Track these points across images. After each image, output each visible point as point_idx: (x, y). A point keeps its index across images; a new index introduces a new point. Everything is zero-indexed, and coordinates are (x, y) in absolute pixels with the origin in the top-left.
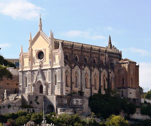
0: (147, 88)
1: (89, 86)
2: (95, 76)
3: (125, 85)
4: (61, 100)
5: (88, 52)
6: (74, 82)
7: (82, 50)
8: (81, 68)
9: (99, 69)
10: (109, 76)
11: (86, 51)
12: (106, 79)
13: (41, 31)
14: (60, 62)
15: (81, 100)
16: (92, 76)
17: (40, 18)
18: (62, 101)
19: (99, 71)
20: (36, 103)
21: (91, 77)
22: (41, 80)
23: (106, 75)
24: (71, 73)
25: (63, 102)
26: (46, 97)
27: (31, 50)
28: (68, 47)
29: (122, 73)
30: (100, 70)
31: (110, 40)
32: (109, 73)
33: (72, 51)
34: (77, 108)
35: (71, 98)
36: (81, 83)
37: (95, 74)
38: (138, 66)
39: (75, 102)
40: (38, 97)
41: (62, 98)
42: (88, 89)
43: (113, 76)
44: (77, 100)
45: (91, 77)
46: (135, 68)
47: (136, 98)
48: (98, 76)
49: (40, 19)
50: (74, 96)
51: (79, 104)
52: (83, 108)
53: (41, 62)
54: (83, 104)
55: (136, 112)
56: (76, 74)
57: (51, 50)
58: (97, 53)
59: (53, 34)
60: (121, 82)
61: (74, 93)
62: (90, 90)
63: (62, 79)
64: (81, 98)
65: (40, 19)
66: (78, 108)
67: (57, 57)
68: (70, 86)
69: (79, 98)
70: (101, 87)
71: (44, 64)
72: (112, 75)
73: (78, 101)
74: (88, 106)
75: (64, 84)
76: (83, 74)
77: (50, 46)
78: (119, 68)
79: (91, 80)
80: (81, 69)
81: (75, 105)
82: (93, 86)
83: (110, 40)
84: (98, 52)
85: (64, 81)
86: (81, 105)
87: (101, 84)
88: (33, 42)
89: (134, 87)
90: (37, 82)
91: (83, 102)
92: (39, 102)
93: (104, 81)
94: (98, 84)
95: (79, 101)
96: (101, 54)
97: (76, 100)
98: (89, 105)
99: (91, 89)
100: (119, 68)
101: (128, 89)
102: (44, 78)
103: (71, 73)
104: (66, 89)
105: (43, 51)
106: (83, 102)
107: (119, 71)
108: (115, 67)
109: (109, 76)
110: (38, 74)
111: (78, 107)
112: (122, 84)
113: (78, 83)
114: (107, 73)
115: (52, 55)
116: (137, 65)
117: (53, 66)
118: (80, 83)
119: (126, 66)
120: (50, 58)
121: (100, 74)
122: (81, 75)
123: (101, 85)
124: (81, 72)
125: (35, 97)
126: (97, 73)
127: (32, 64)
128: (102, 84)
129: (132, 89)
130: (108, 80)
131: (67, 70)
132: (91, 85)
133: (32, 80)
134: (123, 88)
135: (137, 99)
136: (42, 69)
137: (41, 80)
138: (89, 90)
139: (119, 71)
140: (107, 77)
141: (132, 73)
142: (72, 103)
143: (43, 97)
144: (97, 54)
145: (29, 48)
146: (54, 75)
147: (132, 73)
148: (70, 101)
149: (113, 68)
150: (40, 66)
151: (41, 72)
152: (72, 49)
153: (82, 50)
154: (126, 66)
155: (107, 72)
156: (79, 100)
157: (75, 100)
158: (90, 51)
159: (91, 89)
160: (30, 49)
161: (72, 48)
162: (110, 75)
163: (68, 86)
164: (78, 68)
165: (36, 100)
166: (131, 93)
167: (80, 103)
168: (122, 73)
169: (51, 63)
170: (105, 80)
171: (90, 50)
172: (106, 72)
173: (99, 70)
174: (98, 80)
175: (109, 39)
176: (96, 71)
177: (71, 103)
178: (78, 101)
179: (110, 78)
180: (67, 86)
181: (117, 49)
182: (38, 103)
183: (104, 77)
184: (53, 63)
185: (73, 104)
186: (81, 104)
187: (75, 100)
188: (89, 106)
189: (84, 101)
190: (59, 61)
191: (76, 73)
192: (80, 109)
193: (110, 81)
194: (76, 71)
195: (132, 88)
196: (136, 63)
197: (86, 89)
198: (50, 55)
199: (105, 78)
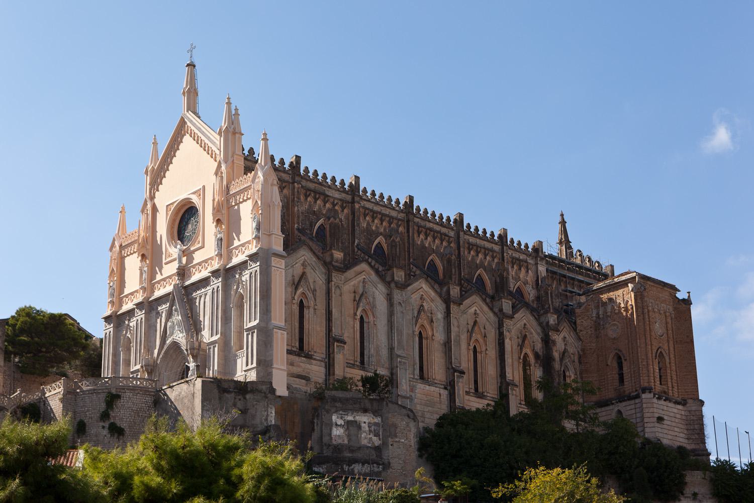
0: (742, 431)
1: (438, 370)
2: (470, 333)
3: (628, 387)
5: (443, 237)
6: (346, 337)
7: (408, 221)
8: (388, 279)
9: (497, 304)
10: (547, 342)
11: (431, 230)
12: (537, 356)
13: (190, 115)
14: (258, 229)
15: (378, 420)
16: (454, 329)
19: (495, 313)
20: (105, 432)
21: (448, 331)
22: (180, 337)
23: (535, 337)
24: (328, 292)
25: (254, 417)
26: (165, 394)
27: (150, 212)
28: (330, 193)
29: (613, 331)
30: (501, 310)
31: (564, 232)
32: (546, 329)
33: (353, 213)
35: (316, 409)
36: (391, 349)
37: (475, 322)
38: (687, 302)
39: (337, 432)
40: (118, 397)
41: (248, 396)
42: (433, 388)
43: (571, 350)
44: (350, 418)
45: (448, 331)
46: (675, 309)
47: (689, 447)
48: (492, 334)
49: (191, 65)
50: (334, 399)
51: (364, 442)
52: (387, 466)
53: (184, 253)
54: (385, 444)
55: (688, 491)
56: (357, 302)
57: (225, 183)
58: (492, 250)
59: (237, 114)
60: (613, 375)
61: (343, 384)
62: (445, 393)
63: (266, 311)
64: (376, 413)
66: (356, 461)
67: (246, 210)
68: (320, 351)
69: (365, 411)
70: (508, 384)
71: (198, 257)
72: (562, 340)
73: (359, 427)
74: (414, 454)
75: (281, 342)
76: (397, 309)
77: (219, 166)
79: (447, 345)
80: (388, 284)
81: (338, 449)
82: (462, 372)
83: (564, 232)
84: (497, 248)
85: (279, 316)
86: (378, 449)
88: (157, 176)
89: (674, 393)
90: (165, 347)
91: (387, 431)
92: (124, 425)
93: (526, 363)
94: (490, 370)
95: (365, 427)
96: (513, 258)
97: (349, 423)
98: (419, 450)
99: (450, 386)
100: (598, 314)
101: (644, 396)
102: (193, 325)
103: (328, 292)
104: (296, 370)
105: (195, 199)
106: (387, 431)
107: (598, 325)
108: (577, 311)
109: (547, 342)
110: (170, 315)
111: (359, 455)
112: (616, 383)
113: (370, 349)
114: (539, 330)
115: (230, 207)
116: (680, 296)
117: (230, 259)
118: (384, 352)
119: (626, 297)
120: (218, 222)
121: (500, 325)
122: (391, 314)
123: (509, 376)
124: (389, 298)
125: (102, 397)
126: (482, 320)
127: (152, 275)
128: (514, 373)
130: (546, 360)
131: (304, 274)
132: (453, 371)
133: (149, 349)
134: (622, 398)
135: (693, 451)
136: (187, 283)
137: (180, 337)
138: (438, 393)
139: (598, 325)
140: (539, 346)
141: (658, 328)
142: (321, 438)
144: (493, 258)
145: (145, 204)
146: (234, 299)
147: (658, 328)
148: (313, 423)
149: (568, 314)
150: (183, 273)
151: (181, 301)
153: (408, 221)
154: (626, 297)
155: (540, 324)
156: (364, 419)
157: (340, 422)
158: (452, 234)
159: (450, 386)
160: (149, 206)
161: (353, 202)
162: (554, 336)
163: (309, 357)
164: (374, 276)
165: (105, 416)
166: (660, 419)
167: (367, 438)
168: (613, 331)
169: (225, 245)
171: (452, 229)
172: (534, 323)
173: (496, 310)
174: (492, 353)
175: (559, 227)
176: (475, 306)
177: (315, 435)
178: (357, 425)
179: (556, 355)
180: (300, 349)
181: (585, 254)
183: (521, 346)
184: (230, 242)
185: (326, 439)
186: (377, 441)
187: (340, 422)
188: (420, 456)
189: (395, 426)
190: (254, 225)
191: (359, 298)
192: (366, 468)
193: (557, 366)
194: (360, 290)
195: (663, 396)
196: (674, 289)
197: (421, 387)
198: (217, 210)
199: (528, 350)
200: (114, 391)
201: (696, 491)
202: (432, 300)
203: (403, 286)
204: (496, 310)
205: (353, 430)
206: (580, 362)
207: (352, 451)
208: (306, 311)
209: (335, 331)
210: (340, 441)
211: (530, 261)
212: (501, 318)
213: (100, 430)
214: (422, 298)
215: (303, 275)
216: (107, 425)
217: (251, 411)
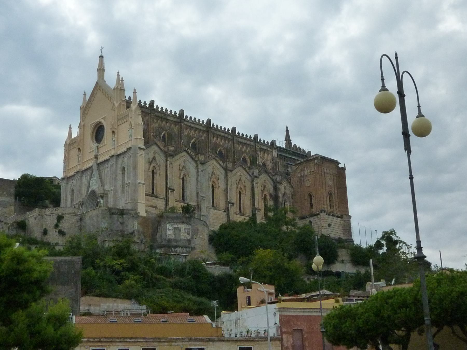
1: (221, 202)
3: (315, 210)
4: (120, 220)
12: (271, 195)
15: (189, 227)
17: (100, 55)
18: (122, 224)
20: (57, 234)
23: (270, 187)
25: (127, 226)
28: (169, 118)
34: (175, 247)
37: (240, 180)
38: (343, 169)
41: (124, 216)
43: (288, 192)
44: (175, 226)
54: (192, 238)
55: (340, 259)
60: (307, 204)
65: (101, 57)
69: (183, 223)
70: (256, 209)
73: (180, 230)
78: (301, 174)
79: (226, 190)
80: (196, 162)
81: (169, 241)
84: (253, 144)
86: (189, 241)
87: (256, 202)
92: (65, 230)
94: (247, 202)
95: (183, 230)
98: (209, 241)
99: (227, 211)
100: (301, 174)
109: (276, 189)
111: (180, 244)
116: (340, 166)
118: (195, 195)
123: (256, 205)
126: (243, 178)
129: (333, 215)
132: (229, 204)
140: (272, 191)
143: (78, 218)
152: (181, 125)
155: (273, 180)
156: (183, 227)
157: (171, 228)
159: (227, 211)
163: (157, 197)
165: (56, 226)
167: (184, 236)
170: (268, 197)
174: (249, 193)
177: (158, 235)
179: (280, 195)
182: (62, 233)
183: (263, 191)
186: (189, 237)
187: (171, 228)
188: (210, 244)
191: (182, 168)
196: (337, 163)
197: (212, 211)
200: (60, 214)
201: (343, 259)
202: (218, 169)
203: (203, 164)
204: (251, 174)
205: (177, 232)
206: (292, 198)
207: (176, 241)
208: (155, 175)
209: (169, 185)
210: (170, 237)
211: (269, 150)
212: (253, 178)
213: (54, 233)
214: (213, 168)
215: (154, 158)
216: (57, 231)
217: (126, 223)
